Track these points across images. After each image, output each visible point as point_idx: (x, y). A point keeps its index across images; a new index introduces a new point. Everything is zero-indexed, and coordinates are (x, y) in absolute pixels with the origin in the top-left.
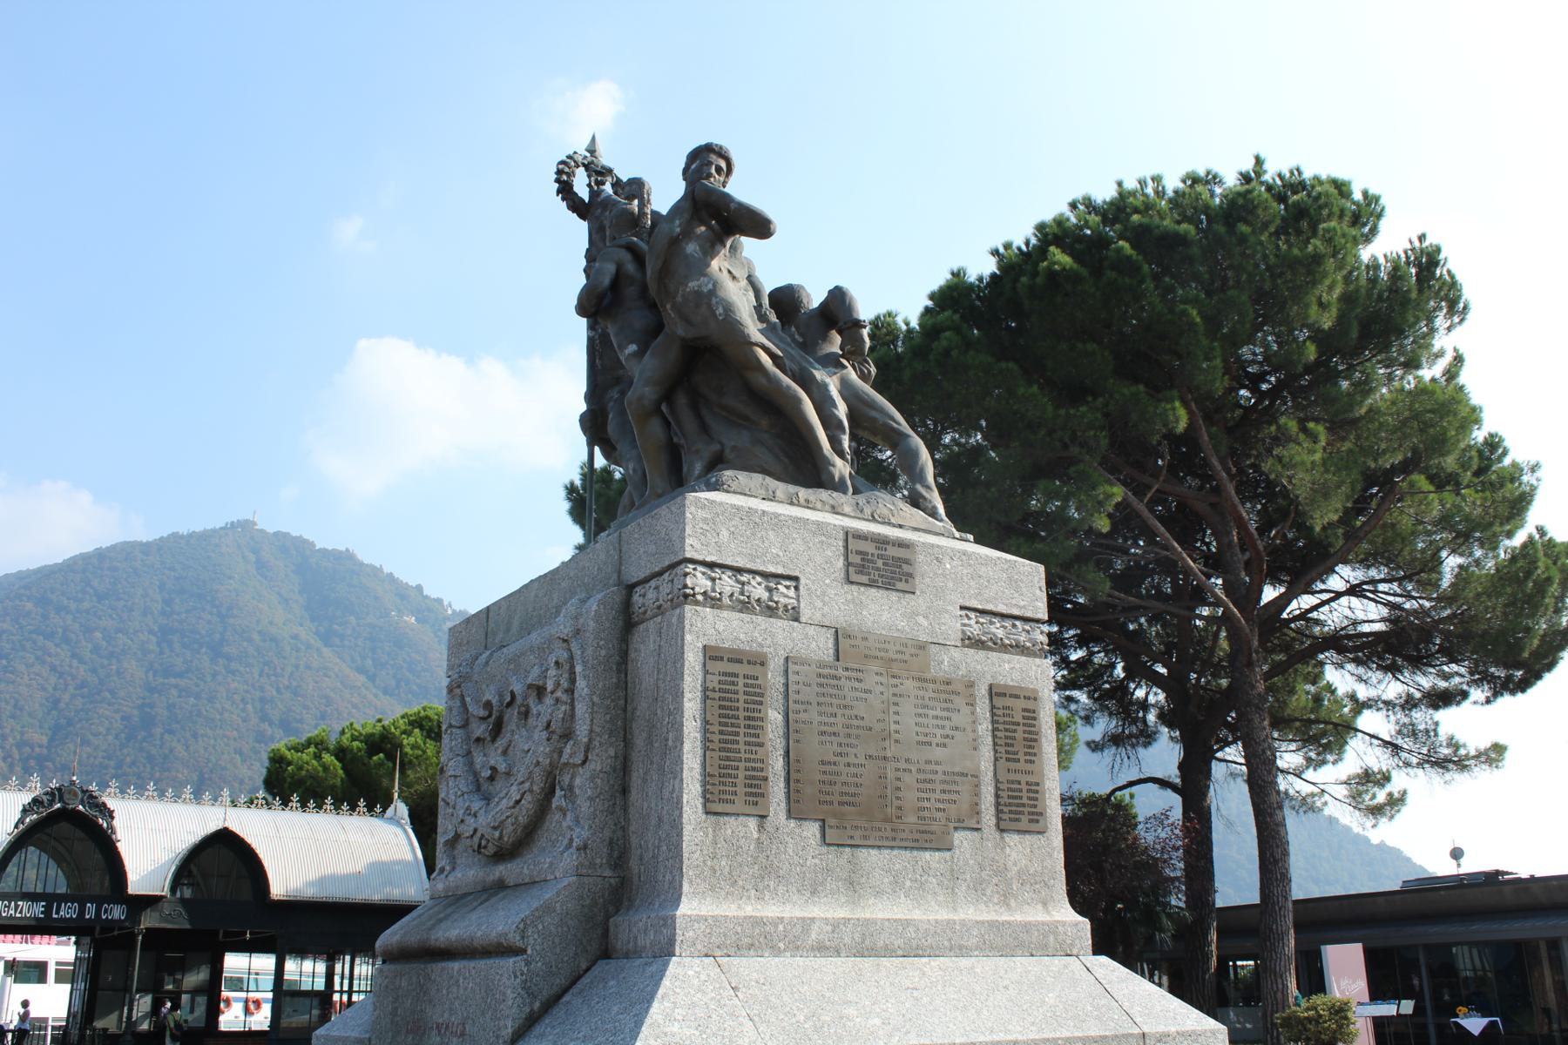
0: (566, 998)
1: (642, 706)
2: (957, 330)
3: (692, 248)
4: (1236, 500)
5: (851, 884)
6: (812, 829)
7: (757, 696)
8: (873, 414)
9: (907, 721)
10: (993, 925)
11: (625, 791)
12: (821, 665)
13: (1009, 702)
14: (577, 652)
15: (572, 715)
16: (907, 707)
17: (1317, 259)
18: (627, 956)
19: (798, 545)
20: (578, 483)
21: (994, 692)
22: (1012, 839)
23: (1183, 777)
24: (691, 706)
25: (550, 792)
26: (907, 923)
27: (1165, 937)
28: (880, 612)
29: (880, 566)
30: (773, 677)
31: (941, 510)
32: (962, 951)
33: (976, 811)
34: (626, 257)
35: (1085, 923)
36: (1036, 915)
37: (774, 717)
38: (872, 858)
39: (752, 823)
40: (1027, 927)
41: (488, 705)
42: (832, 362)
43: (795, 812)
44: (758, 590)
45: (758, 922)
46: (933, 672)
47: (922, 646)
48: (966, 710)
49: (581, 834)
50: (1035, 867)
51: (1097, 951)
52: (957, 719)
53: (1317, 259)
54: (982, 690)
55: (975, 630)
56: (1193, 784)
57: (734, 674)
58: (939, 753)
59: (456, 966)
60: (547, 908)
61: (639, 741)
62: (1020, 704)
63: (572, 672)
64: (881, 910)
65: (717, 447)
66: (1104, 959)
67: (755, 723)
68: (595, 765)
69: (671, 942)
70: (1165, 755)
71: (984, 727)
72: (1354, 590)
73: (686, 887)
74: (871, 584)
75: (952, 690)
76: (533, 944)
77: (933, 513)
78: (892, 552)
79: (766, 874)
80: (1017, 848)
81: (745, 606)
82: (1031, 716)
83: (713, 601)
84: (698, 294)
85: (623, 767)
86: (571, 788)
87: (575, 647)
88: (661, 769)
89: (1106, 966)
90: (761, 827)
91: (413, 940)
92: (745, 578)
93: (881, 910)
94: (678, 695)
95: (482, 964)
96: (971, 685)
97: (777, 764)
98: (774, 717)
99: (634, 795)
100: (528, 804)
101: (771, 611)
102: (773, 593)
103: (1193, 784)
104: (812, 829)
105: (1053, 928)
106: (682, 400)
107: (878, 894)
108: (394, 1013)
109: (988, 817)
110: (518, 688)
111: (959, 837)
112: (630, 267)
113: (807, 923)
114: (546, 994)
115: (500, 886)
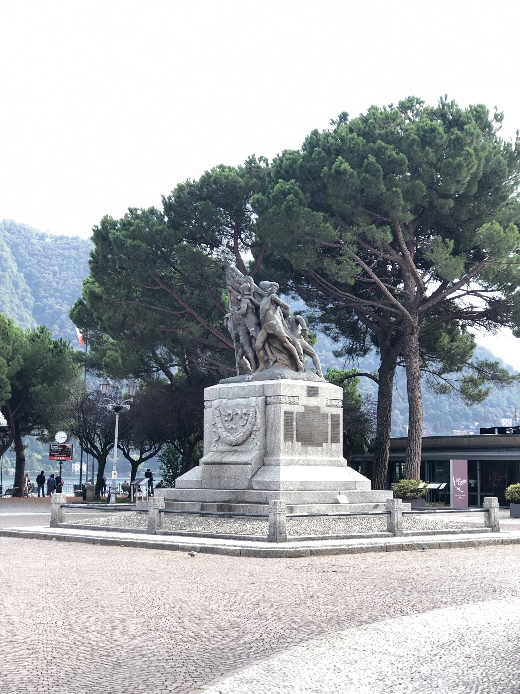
0: (258, 472)
1: (270, 420)
2: (296, 194)
3: (271, 312)
4: (414, 266)
5: (306, 453)
6: (300, 443)
7: (292, 420)
8: (308, 350)
9: (316, 423)
10: (330, 461)
11: (266, 435)
12: (302, 413)
13: (334, 417)
14: (257, 409)
15: (256, 420)
16: (316, 420)
17: (459, 166)
18: (268, 465)
19: (299, 390)
20: (100, 227)
21: (332, 416)
22: (333, 444)
23: (380, 376)
24: (282, 423)
25: (251, 435)
26: (315, 460)
27: (430, 406)
28: (313, 402)
29: (313, 392)
30: (295, 416)
31: (322, 376)
32: (324, 465)
33: (327, 439)
34: (249, 301)
35: (346, 460)
36: (336, 459)
37: (295, 423)
38: (310, 448)
39: (291, 443)
40: (335, 461)
41: (230, 414)
42: (299, 337)
43: (298, 440)
44: (292, 400)
45: (292, 460)
46: (321, 412)
47: (319, 408)
48: (326, 419)
49: (259, 444)
50: (337, 449)
51: (348, 466)
52: (325, 422)
53: (459, 166)
54: (329, 415)
55: (329, 404)
56: (384, 379)
57: (288, 415)
58: (321, 428)
59: (232, 466)
60: (254, 457)
61: (269, 427)
62: (336, 418)
63: (256, 412)
64: (311, 458)
65: (275, 359)
66: (349, 468)
67: (292, 424)
68: (261, 431)
69: (279, 463)
70: (372, 361)
71: (330, 423)
72: (475, 293)
73: (281, 454)
74: (311, 396)
75: (325, 416)
76: (253, 463)
77: (321, 377)
78: (315, 389)
79: (293, 451)
80: (334, 445)
81: (290, 403)
82: (338, 420)
83: (285, 403)
84: (273, 324)
85: (266, 431)
86: (255, 434)
87: (256, 408)
88: (275, 433)
89: (349, 468)
90: (292, 443)
91: (210, 460)
92: (290, 398)
93: (311, 458)
94: (279, 420)
95: (241, 466)
96: (327, 414)
97: (295, 432)
98: (295, 423)
99: (268, 436)
100: (245, 437)
101: (294, 404)
102: (294, 400)
103: (384, 379)
104: (300, 443)
105: (340, 461)
106: (267, 346)
107: (310, 455)
108: (211, 475)
109: (329, 440)
110: (239, 412)
111: (324, 444)
112: (250, 305)
113: (299, 460)
114: (255, 471)
115: (236, 451)
